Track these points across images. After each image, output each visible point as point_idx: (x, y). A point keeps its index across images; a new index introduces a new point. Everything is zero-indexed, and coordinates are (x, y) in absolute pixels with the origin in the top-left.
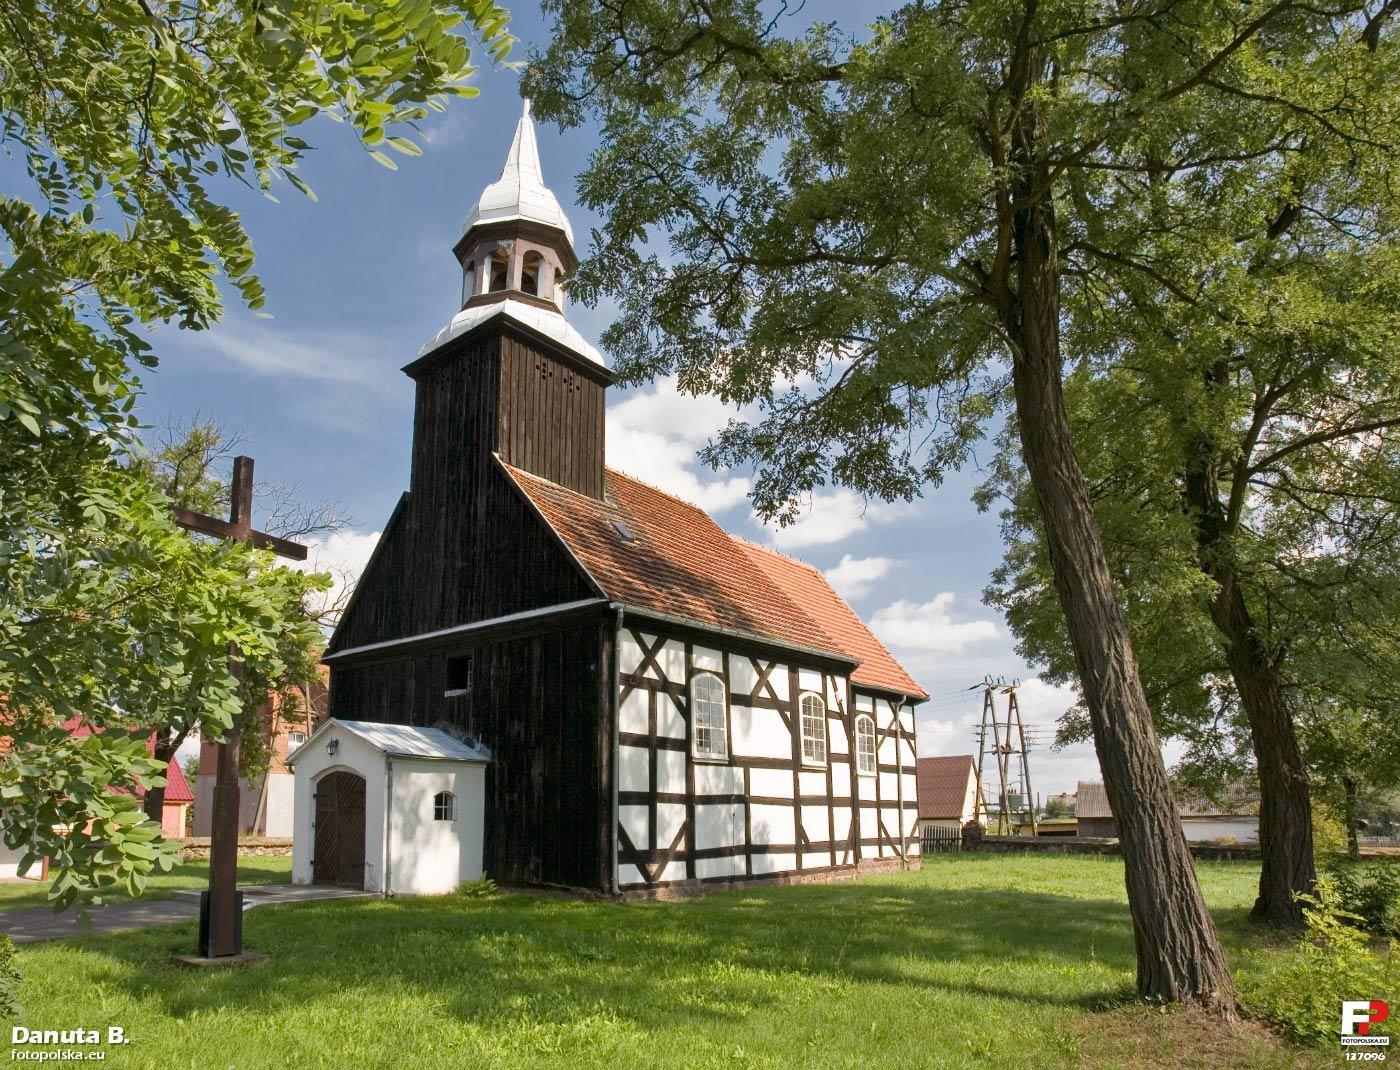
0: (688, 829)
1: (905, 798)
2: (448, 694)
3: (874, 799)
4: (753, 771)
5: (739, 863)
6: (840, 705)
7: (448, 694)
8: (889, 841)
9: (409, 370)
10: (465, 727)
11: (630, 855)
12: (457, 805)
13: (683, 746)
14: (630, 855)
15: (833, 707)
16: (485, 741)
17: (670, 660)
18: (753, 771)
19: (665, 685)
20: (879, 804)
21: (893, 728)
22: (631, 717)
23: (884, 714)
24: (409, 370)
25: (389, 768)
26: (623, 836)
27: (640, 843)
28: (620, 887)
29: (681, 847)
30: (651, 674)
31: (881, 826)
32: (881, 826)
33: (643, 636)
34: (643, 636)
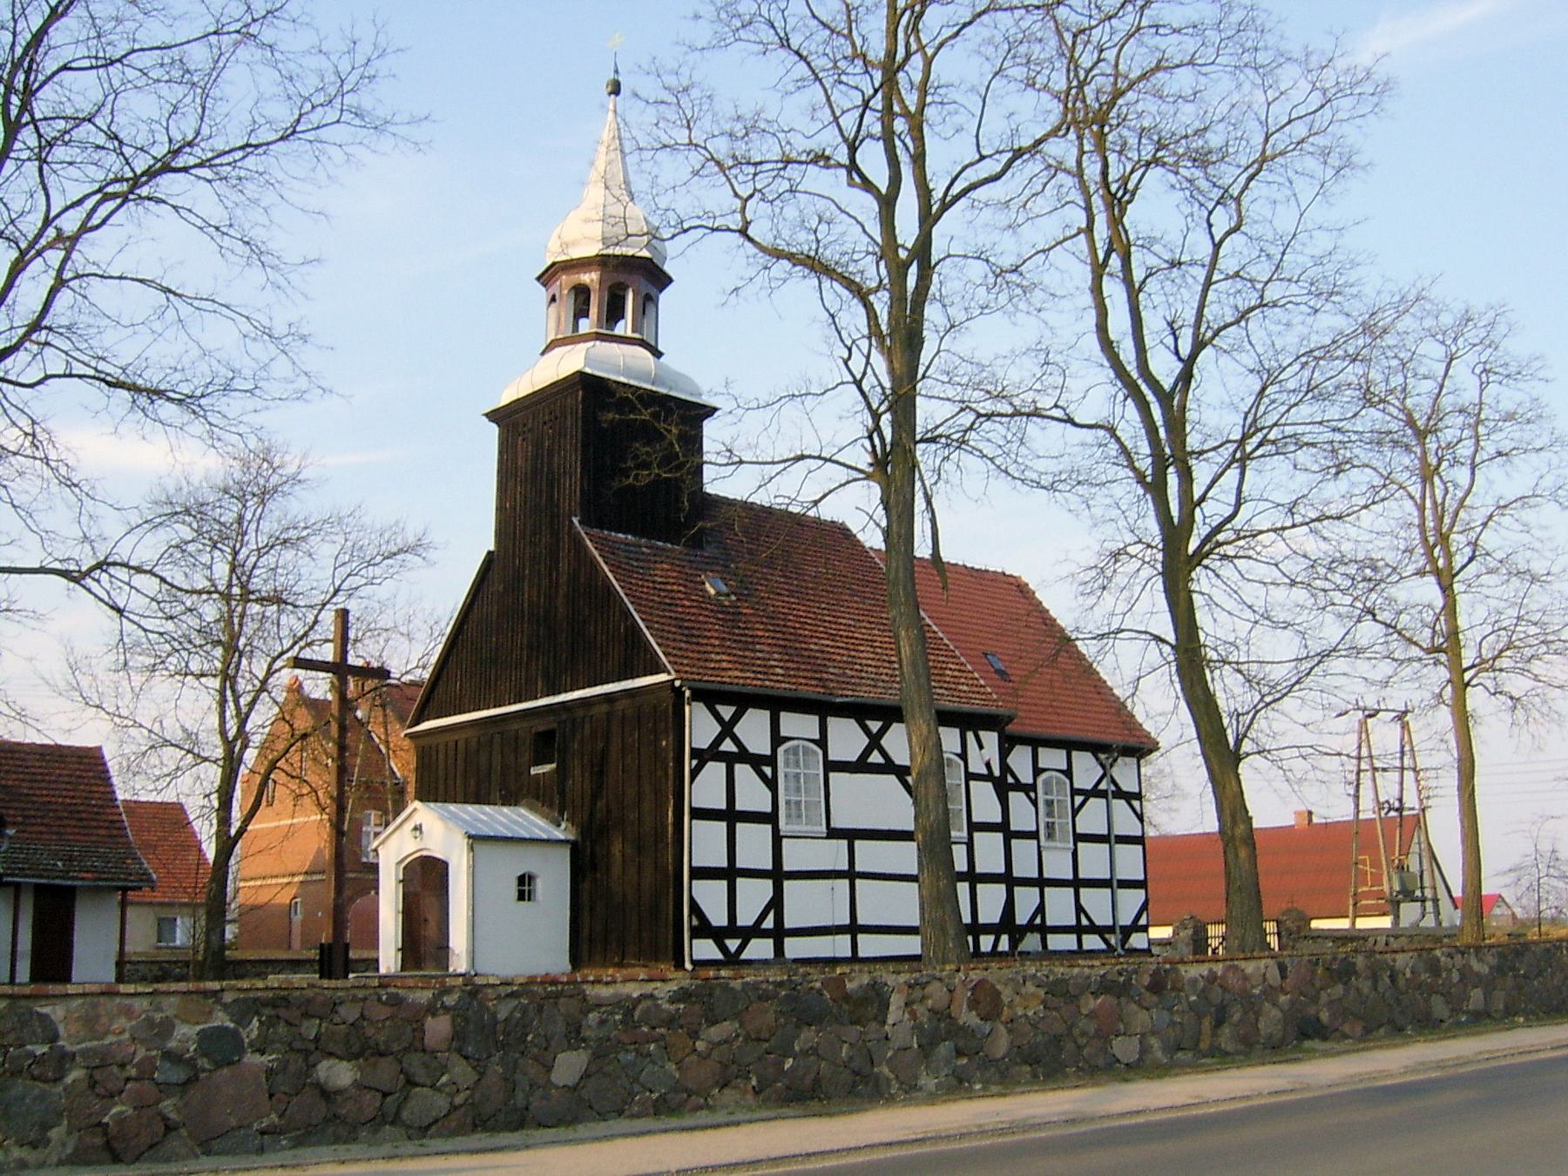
0: (776, 903)
1: (1121, 875)
2: (534, 771)
3: (1070, 876)
4: (858, 843)
5: (840, 946)
6: (988, 765)
7: (534, 771)
8: (1093, 929)
9: (494, 416)
10: (551, 806)
11: (704, 929)
12: (540, 886)
13: (771, 818)
14: (704, 929)
15: (977, 767)
16: (571, 820)
17: (754, 730)
18: (858, 843)
19: (743, 756)
20: (1041, 882)
21: (1103, 786)
22: (707, 788)
23: (1086, 770)
24: (494, 416)
25: (471, 848)
26: (695, 909)
27: (718, 918)
28: (693, 962)
29: (769, 923)
30: (728, 746)
31: (1080, 909)
32: (1080, 909)
33: (719, 708)
34: (719, 708)
